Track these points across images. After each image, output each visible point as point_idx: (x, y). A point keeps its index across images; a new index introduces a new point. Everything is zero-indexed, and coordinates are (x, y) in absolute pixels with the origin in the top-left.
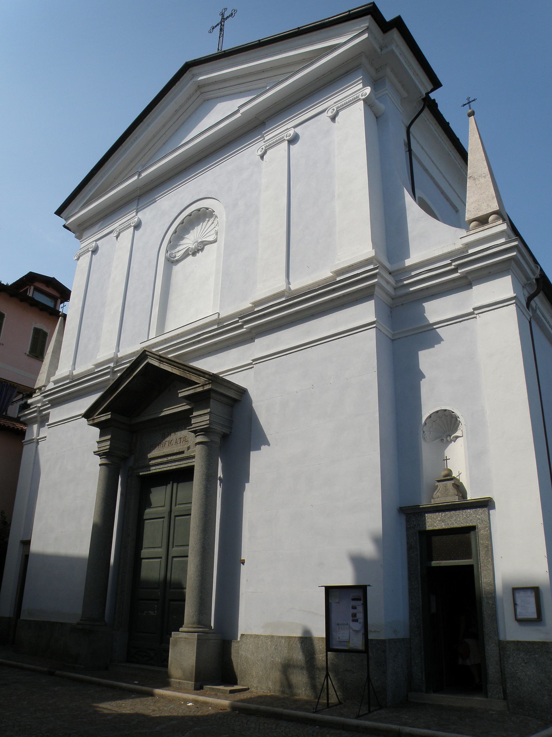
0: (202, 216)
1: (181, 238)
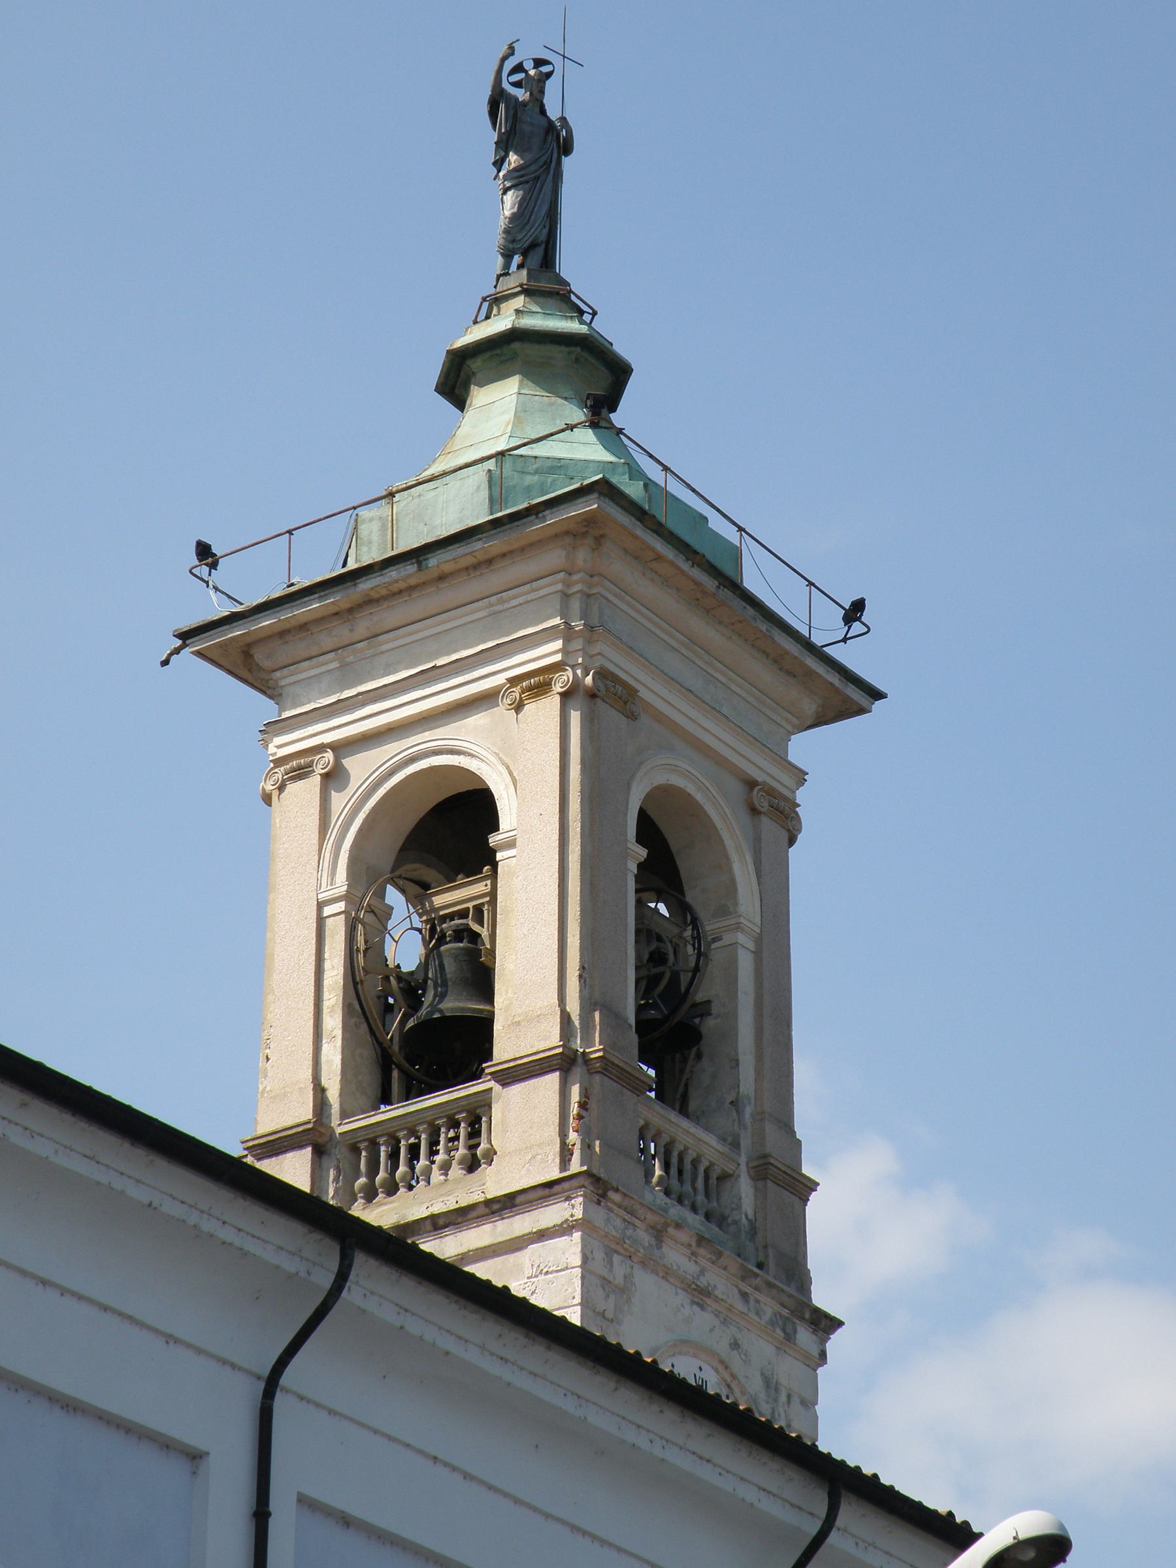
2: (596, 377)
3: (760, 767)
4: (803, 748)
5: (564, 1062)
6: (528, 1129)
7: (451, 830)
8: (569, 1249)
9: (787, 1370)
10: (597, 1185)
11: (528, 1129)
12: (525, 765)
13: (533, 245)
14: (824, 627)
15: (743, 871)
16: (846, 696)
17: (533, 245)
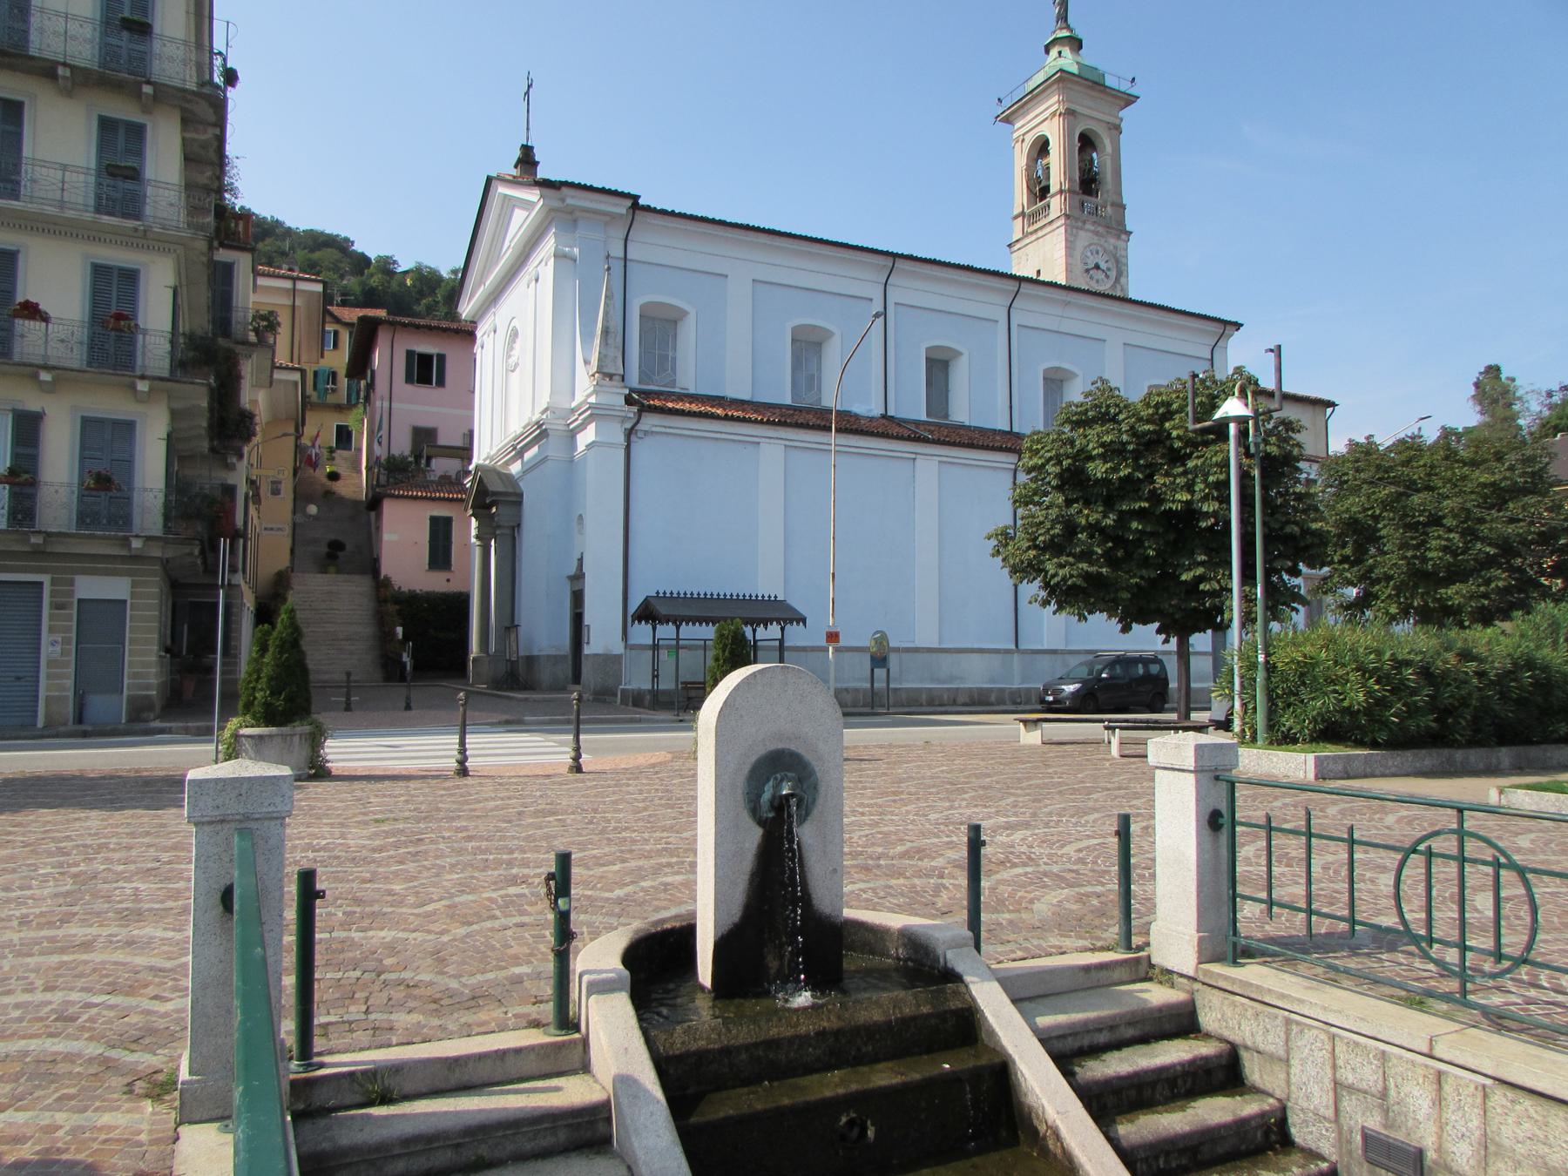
0: (514, 335)
1: (512, 349)
2: (1076, 44)
3: (1111, 120)
4: (1121, 114)
5: (1061, 192)
6: (1056, 204)
7: (1042, 147)
8: (1062, 230)
9: (1120, 244)
10: (1067, 217)
11: (1056, 204)
12: (1054, 131)
13: (1063, 17)
14: (1124, 87)
15: (1107, 142)
16: (1129, 100)
17: (1063, 17)
